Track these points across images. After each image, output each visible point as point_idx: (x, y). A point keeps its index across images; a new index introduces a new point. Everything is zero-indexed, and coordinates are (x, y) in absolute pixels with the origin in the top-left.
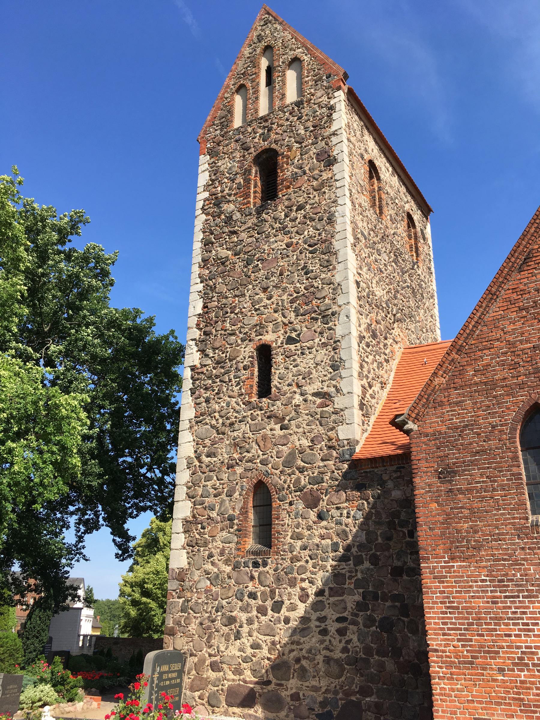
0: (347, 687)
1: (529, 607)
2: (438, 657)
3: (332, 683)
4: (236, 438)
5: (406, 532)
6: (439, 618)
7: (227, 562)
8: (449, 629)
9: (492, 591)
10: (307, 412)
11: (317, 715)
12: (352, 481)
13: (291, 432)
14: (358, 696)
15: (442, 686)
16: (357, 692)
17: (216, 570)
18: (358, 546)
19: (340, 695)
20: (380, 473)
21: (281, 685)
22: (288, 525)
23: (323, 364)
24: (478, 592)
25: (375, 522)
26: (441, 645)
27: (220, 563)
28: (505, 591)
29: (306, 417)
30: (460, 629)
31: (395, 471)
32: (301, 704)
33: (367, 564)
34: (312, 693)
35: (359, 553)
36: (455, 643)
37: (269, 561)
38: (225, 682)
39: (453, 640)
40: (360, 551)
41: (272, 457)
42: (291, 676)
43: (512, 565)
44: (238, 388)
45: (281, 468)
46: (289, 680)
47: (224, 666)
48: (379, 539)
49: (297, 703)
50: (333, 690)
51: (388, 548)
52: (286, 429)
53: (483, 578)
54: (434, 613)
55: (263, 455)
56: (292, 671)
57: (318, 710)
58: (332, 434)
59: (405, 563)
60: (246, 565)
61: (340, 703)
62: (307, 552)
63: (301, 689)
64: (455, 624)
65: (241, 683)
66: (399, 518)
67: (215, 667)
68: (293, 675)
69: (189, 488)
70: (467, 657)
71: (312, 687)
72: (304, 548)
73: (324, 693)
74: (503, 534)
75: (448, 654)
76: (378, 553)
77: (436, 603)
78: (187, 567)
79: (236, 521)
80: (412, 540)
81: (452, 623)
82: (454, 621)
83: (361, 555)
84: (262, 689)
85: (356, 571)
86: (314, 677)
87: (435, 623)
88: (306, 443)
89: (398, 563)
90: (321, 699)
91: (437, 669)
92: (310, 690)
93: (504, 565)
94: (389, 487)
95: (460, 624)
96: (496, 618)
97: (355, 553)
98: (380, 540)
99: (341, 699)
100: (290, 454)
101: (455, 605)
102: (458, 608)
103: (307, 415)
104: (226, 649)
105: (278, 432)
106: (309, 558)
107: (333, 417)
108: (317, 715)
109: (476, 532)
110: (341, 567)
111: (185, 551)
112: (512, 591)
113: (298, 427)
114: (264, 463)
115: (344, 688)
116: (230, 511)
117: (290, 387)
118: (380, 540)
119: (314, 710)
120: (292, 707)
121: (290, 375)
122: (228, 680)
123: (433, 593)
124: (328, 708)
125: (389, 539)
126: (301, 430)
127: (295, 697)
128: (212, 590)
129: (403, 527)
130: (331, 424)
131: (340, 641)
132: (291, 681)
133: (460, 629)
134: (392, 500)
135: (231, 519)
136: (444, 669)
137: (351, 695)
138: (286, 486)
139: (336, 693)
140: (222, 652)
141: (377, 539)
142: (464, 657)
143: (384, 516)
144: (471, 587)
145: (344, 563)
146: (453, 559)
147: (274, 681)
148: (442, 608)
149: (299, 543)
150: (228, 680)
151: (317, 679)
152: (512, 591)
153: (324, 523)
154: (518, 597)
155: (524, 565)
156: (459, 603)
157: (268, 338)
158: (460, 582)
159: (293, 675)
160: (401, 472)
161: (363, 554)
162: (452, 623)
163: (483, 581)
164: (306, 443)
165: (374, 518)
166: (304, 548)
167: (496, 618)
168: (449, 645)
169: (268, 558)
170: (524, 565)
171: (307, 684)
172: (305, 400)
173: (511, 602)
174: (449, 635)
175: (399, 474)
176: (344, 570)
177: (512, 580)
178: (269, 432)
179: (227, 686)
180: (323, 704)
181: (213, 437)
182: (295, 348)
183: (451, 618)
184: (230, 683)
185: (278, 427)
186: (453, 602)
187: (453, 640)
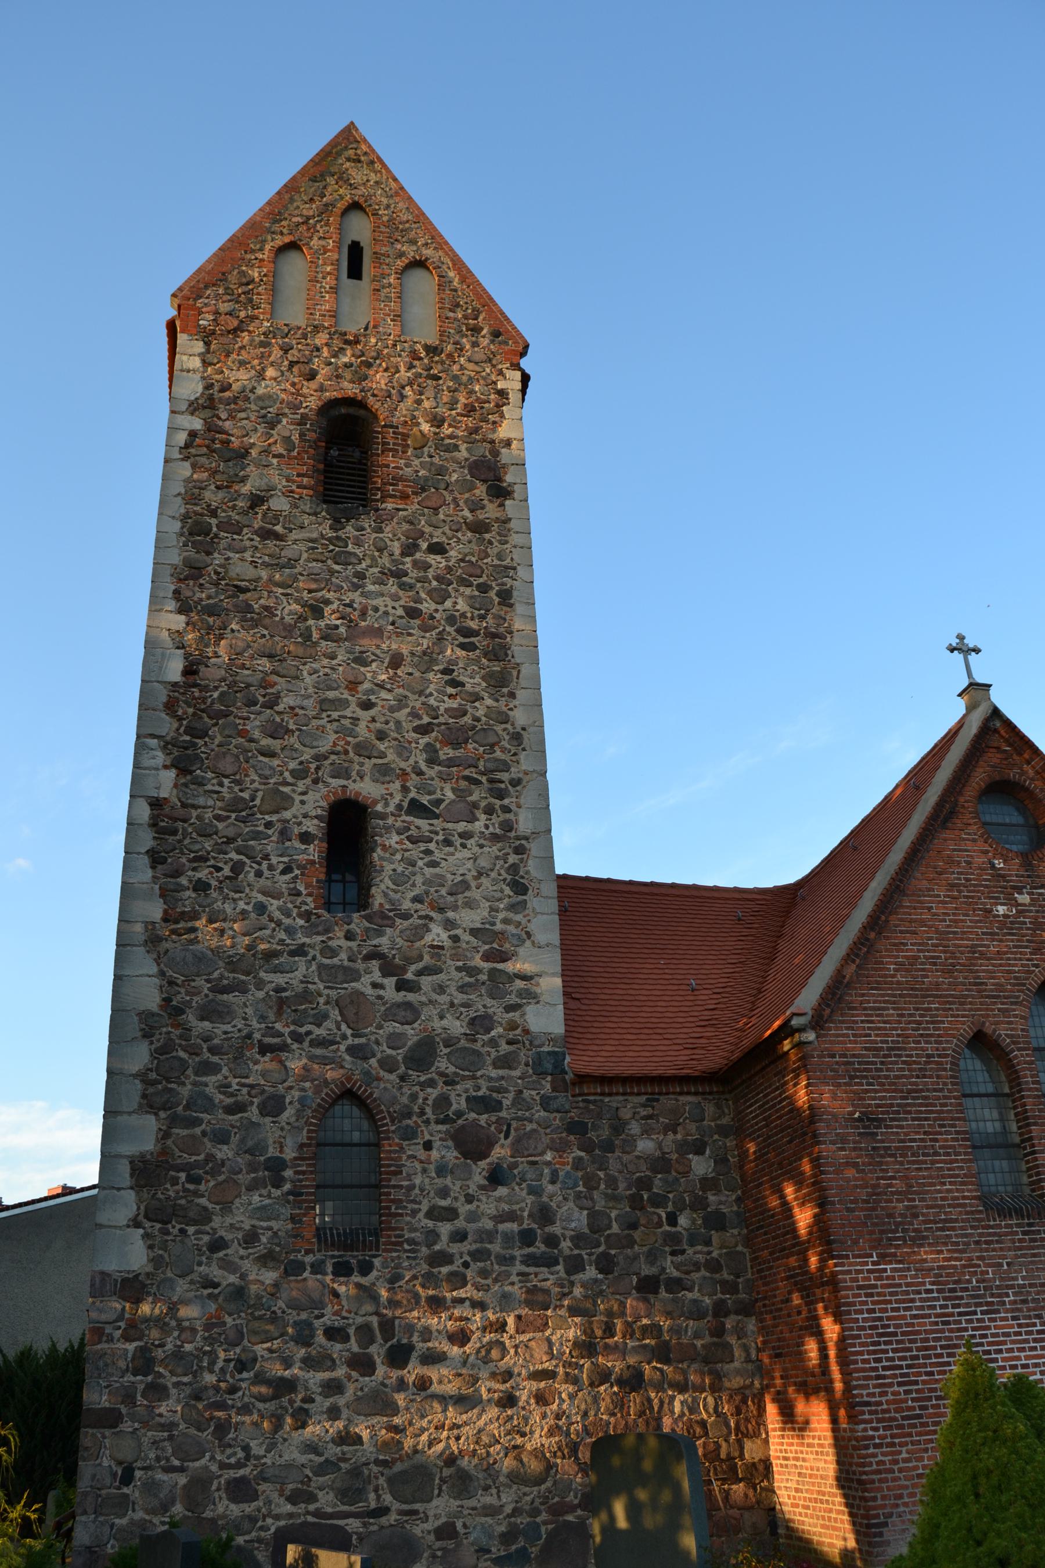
0: (556, 1499)
1: (988, 1328)
2: (870, 1413)
3: (525, 1494)
4: (285, 990)
5: (664, 1215)
6: (869, 1353)
7: (266, 1259)
8: (884, 1368)
9: (942, 1307)
10: (460, 964)
11: (496, 1561)
12: (558, 1115)
13: (424, 999)
14: (579, 1512)
15: (880, 1458)
16: (579, 1506)
17: (233, 1279)
18: (572, 1239)
19: (544, 1516)
20: (615, 1105)
21: (415, 1512)
22: (422, 1190)
23: (493, 875)
24: (922, 1308)
25: (606, 1195)
26: (873, 1395)
27: (246, 1265)
28: (958, 1306)
29: (455, 974)
30: (901, 1367)
31: (644, 1106)
32: (459, 1545)
33: (591, 1272)
34: (483, 1519)
35: (576, 1252)
36: (896, 1388)
37: (377, 1262)
38: (269, 1521)
39: (891, 1385)
40: (577, 1246)
41: (377, 1043)
42: (436, 1492)
43: (964, 1266)
44: (287, 877)
45: (402, 1069)
46: (430, 1500)
47: (263, 1487)
48: (615, 1225)
49: (450, 1544)
50: (527, 1507)
51: (632, 1243)
52: (410, 990)
53: (929, 1287)
54: (862, 1345)
55: (352, 1035)
56: (437, 1481)
57: (497, 1550)
58: (514, 1015)
59: (664, 1269)
60: (317, 1268)
61: (543, 1529)
62: (466, 1247)
63: (458, 1515)
64: (892, 1359)
65: (310, 1519)
66: (649, 1189)
67: (241, 1491)
68: (440, 1490)
69: (147, 1083)
70: (913, 1408)
71: (484, 1507)
72: (459, 1236)
73: (509, 1516)
74: (951, 1221)
75: (885, 1407)
76: (613, 1252)
77: (863, 1328)
78: (149, 1269)
79: (288, 1173)
80: (674, 1229)
81: (888, 1359)
82: (891, 1354)
83: (580, 1255)
84: (365, 1525)
85: (572, 1284)
86: (486, 1488)
87: (864, 1361)
88: (457, 1027)
89: (647, 1270)
90: (503, 1528)
91: (871, 1433)
92: (480, 1515)
93: (954, 1267)
94: (632, 1132)
95: (900, 1359)
96: (948, 1347)
97: (567, 1252)
98: (615, 1228)
99: (545, 1523)
100: (419, 1044)
101: (892, 1330)
102: (895, 1334)
103: (459, 969)
104: (268, 1451)
105: (390, 994)
106: (468, 1259)
107: (519, 984)
108: (496, 1561)
109: (915, 1216)
110: (541, 1277)
111: (141, 1231)
112: (967, 1305)
113: (441, 989)
114: (359, 1052)
115: (551, 1502)
116: (271, 1149)
117: (419, 906)
118: (615, 1228)
119: (489, 1551)
120: (439, 1553)
121: (419, 880)
122: (277, 1517)
123: (857, 1312)
124: (521, 1543)
125: (634, 1226)
126: (443, 999)
127: (446, 1532)
128: (224, 1324)
129: (658, 1207)
130: (513, 999)
131: (544, 1416)
132: (435, 1502)
133: (901, 1367)
134: (638, 1157)
135: (276, 1166)
136: (881, 1432)
137: (567, 1512)
138: (416, 1109)
139: (535, 1512)
140: (258, 1458)
141: (610, 1227)
142: (909, 1409)
143: (622, 1186)
144: (913, 1301)
145: (545, 1269)
146: (883, 1258)
147: (396, 1506)
148: (871, 1336)
149: (445, 1229)
150: (277, 1517)
151: (494, 1491)
152: (967, 1305)
153: (502, 1191)
154: (975, 1313)
155: (979, 1266)
156: (896, 1326)
157: (366, 788)
158: (896, 1294)
159: (440, 1490)
160: (653, 1108)
161: (583, 1253)
162: (888, 1359)
163: (928, 1291)
164: (457, 1027)
165: (602, 1186)
166: (459, 1236)
167: (948, 1347)
168: (885, 1393)
169: (375, 1256)
170: (979, 1266)
171: (472, 1503)
172: (455, 939)
173: (968, 1321)
174: (884, 1377)
175: (650, 1111)
176: (548, 1283)
177: (966, 1289)
178: (369, 991)
179: (273, 1530)
180: (507, 1538)
181: (216, 975)
182: (428, 828)
183: (886, 1351)
184: (282, 1523)
185: (390, 982)
186: (888, 1326)
187: (891, 1385)
